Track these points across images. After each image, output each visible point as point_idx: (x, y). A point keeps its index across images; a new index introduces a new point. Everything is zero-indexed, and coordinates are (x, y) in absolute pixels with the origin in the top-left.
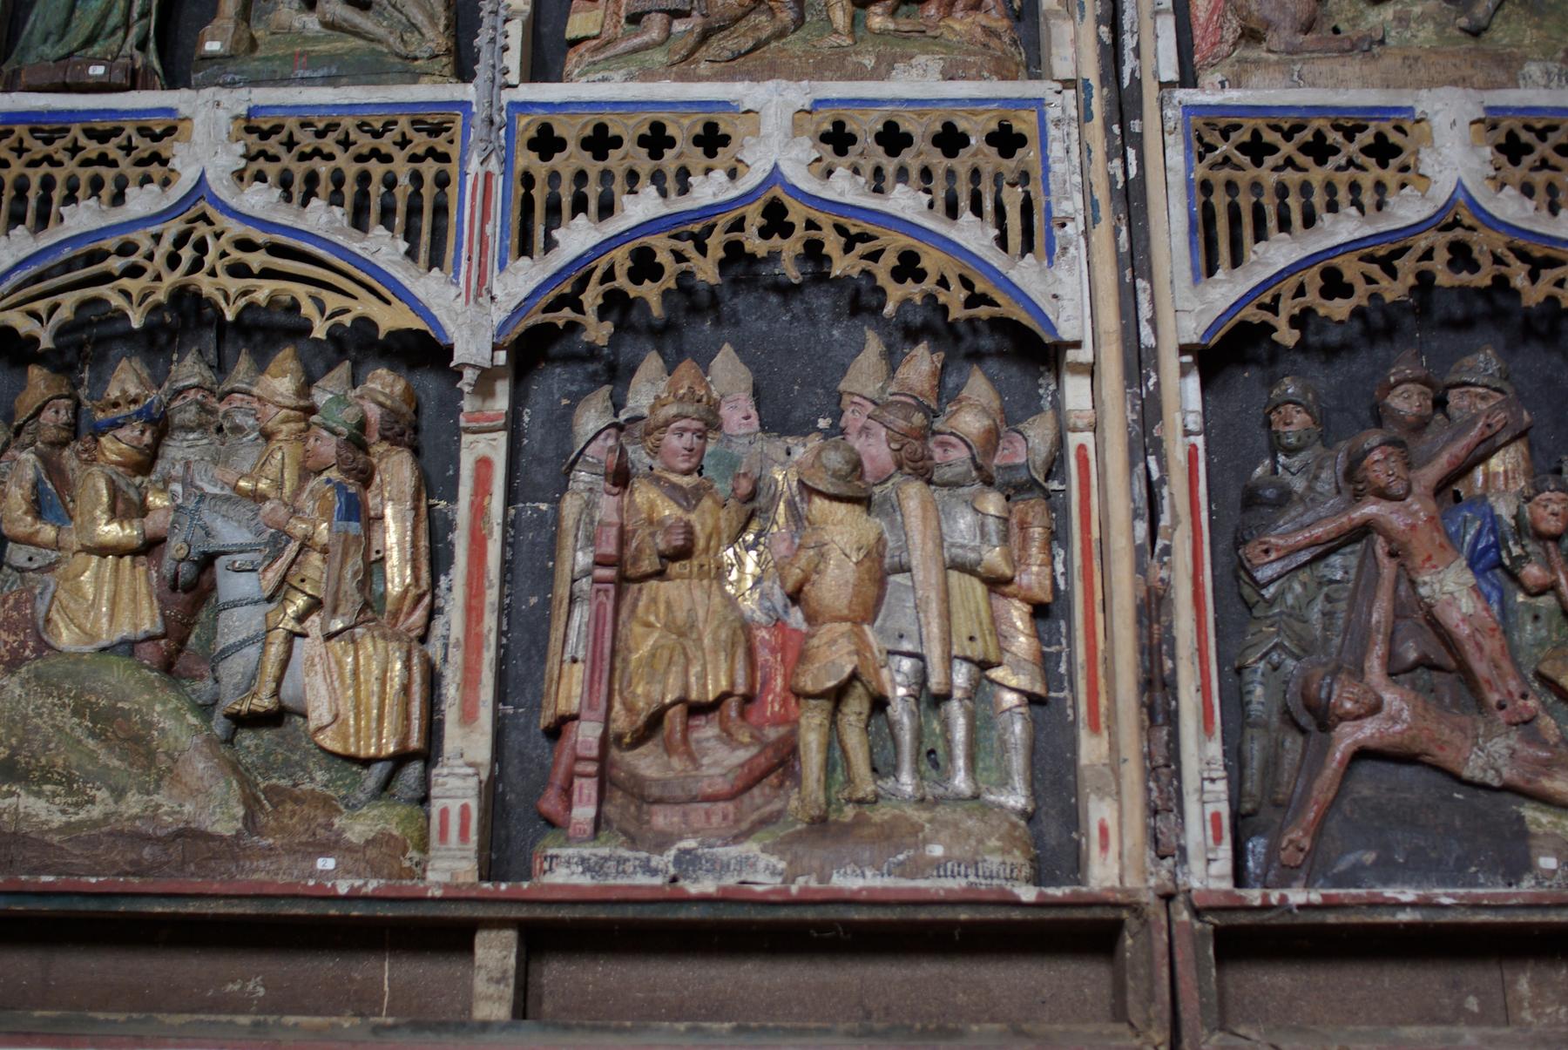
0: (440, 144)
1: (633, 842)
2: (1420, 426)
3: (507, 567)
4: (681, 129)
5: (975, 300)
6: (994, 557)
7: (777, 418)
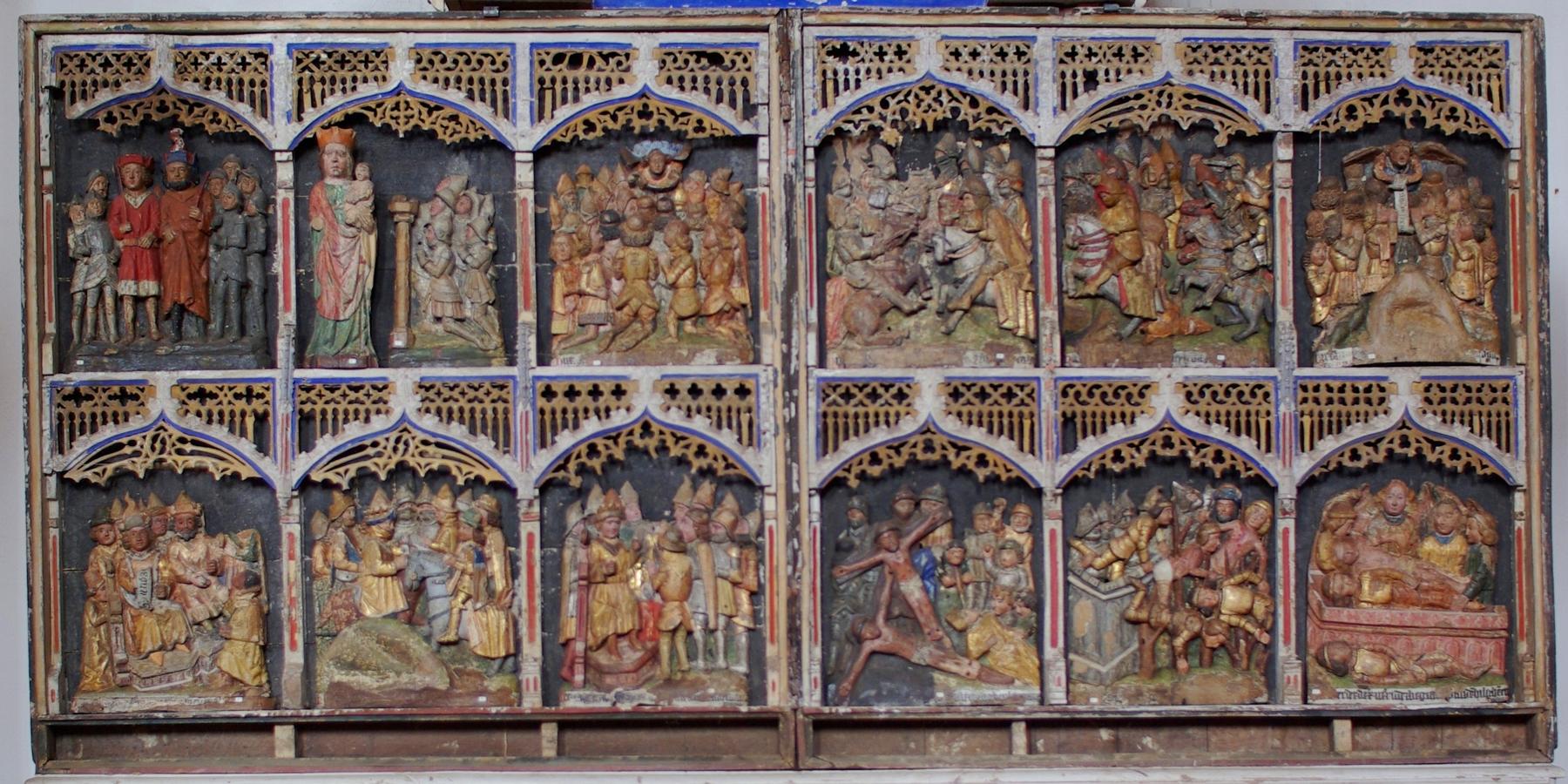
0: (503, 394)
1: (599, 689)
2: (908, 516)
3: (543, 576)
5: (728, 466)
6: (734, 574)
7: (649, 514)
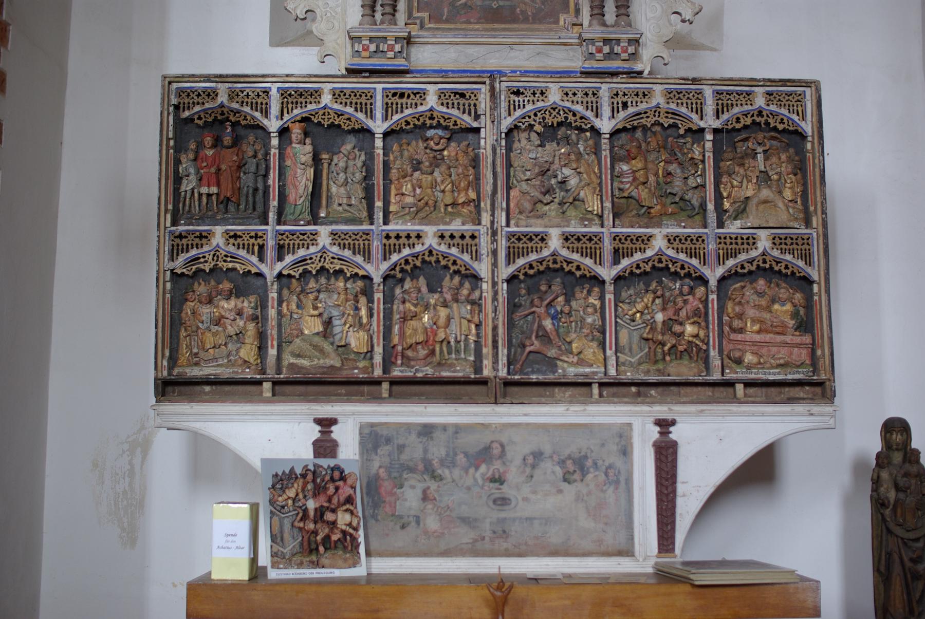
1: (408, 367)
2: (546, 292)
4: (413, 235)
5: (466, 269)
6: (469, 317)
7: (431, 290)
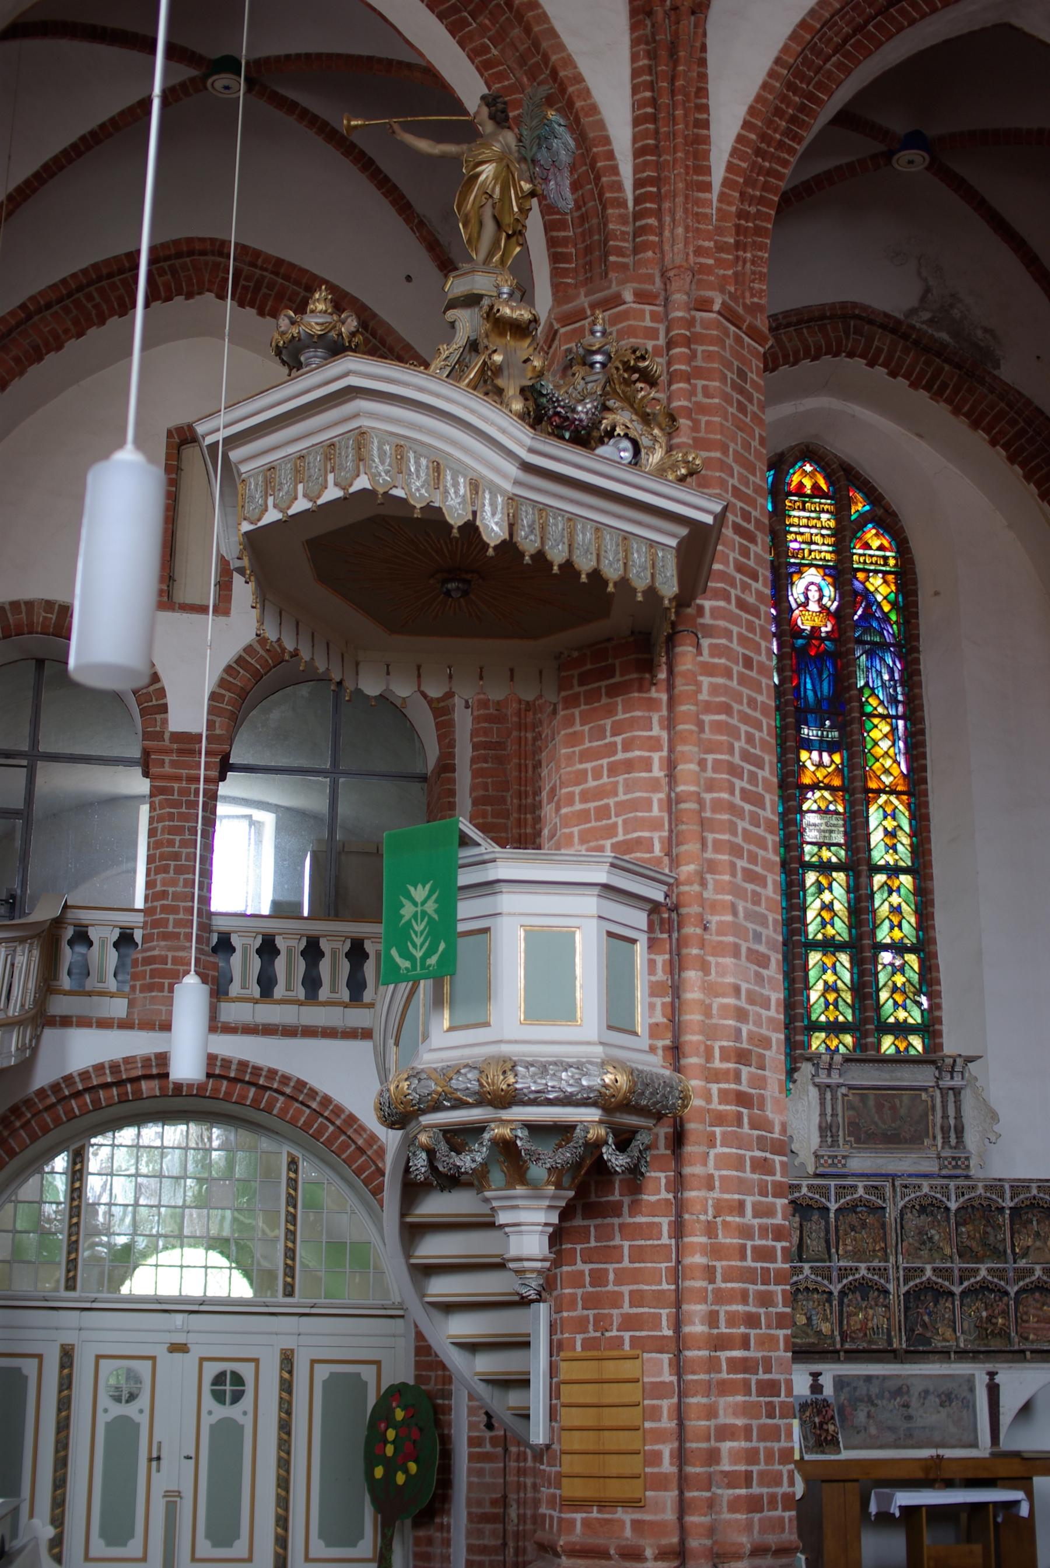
7: (863, 1299)
